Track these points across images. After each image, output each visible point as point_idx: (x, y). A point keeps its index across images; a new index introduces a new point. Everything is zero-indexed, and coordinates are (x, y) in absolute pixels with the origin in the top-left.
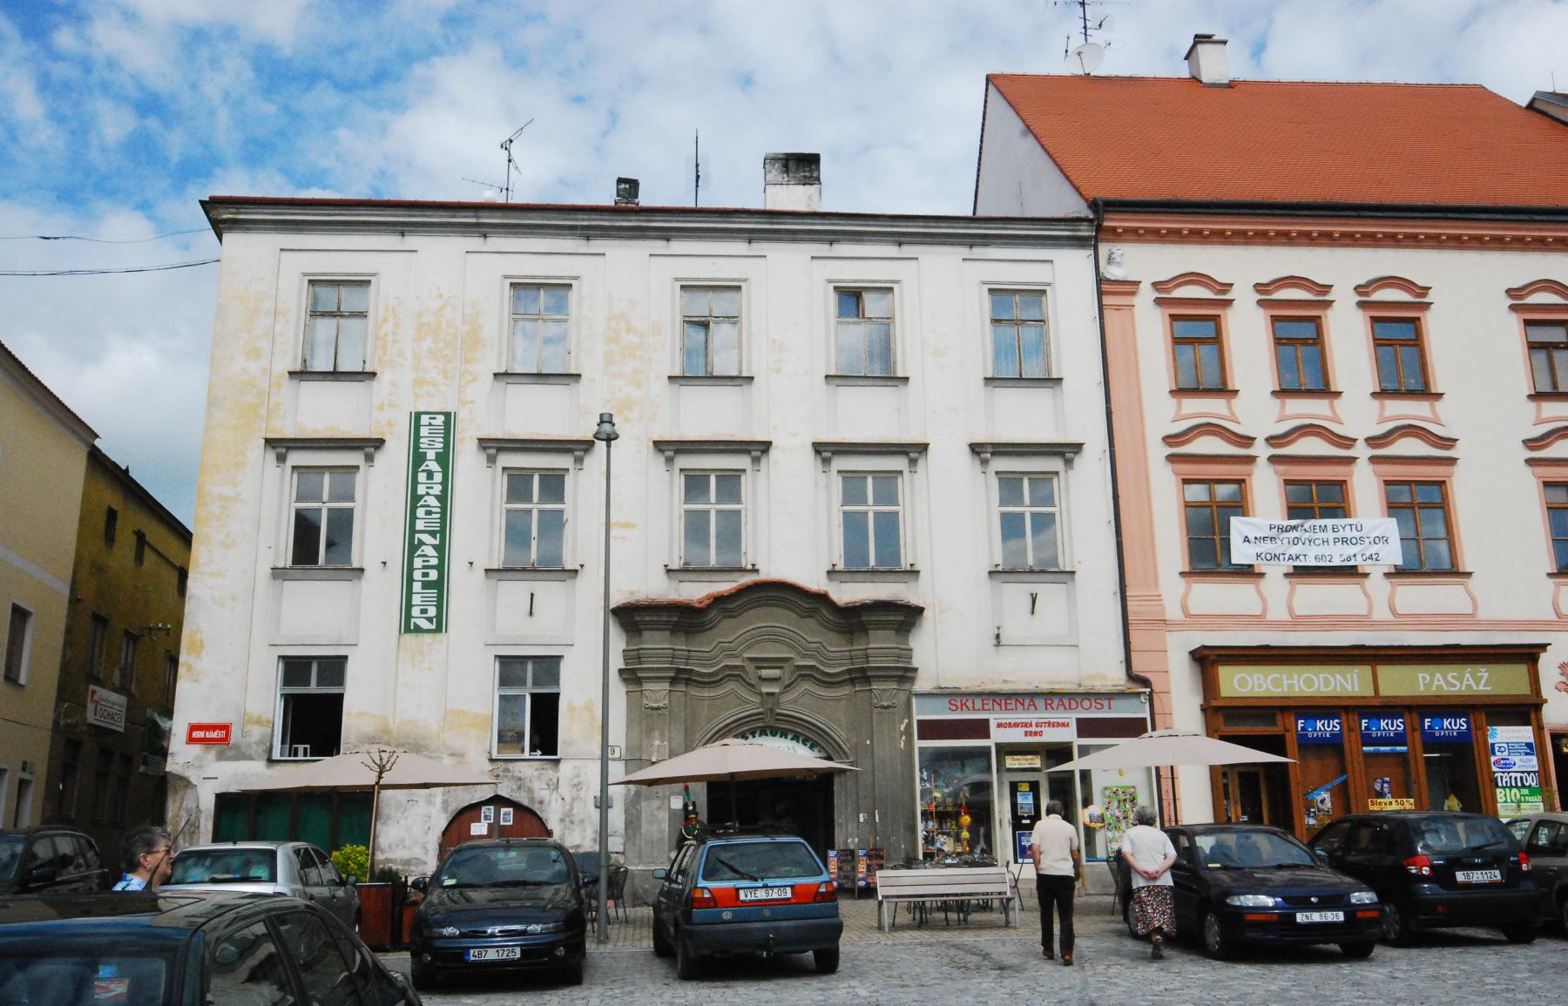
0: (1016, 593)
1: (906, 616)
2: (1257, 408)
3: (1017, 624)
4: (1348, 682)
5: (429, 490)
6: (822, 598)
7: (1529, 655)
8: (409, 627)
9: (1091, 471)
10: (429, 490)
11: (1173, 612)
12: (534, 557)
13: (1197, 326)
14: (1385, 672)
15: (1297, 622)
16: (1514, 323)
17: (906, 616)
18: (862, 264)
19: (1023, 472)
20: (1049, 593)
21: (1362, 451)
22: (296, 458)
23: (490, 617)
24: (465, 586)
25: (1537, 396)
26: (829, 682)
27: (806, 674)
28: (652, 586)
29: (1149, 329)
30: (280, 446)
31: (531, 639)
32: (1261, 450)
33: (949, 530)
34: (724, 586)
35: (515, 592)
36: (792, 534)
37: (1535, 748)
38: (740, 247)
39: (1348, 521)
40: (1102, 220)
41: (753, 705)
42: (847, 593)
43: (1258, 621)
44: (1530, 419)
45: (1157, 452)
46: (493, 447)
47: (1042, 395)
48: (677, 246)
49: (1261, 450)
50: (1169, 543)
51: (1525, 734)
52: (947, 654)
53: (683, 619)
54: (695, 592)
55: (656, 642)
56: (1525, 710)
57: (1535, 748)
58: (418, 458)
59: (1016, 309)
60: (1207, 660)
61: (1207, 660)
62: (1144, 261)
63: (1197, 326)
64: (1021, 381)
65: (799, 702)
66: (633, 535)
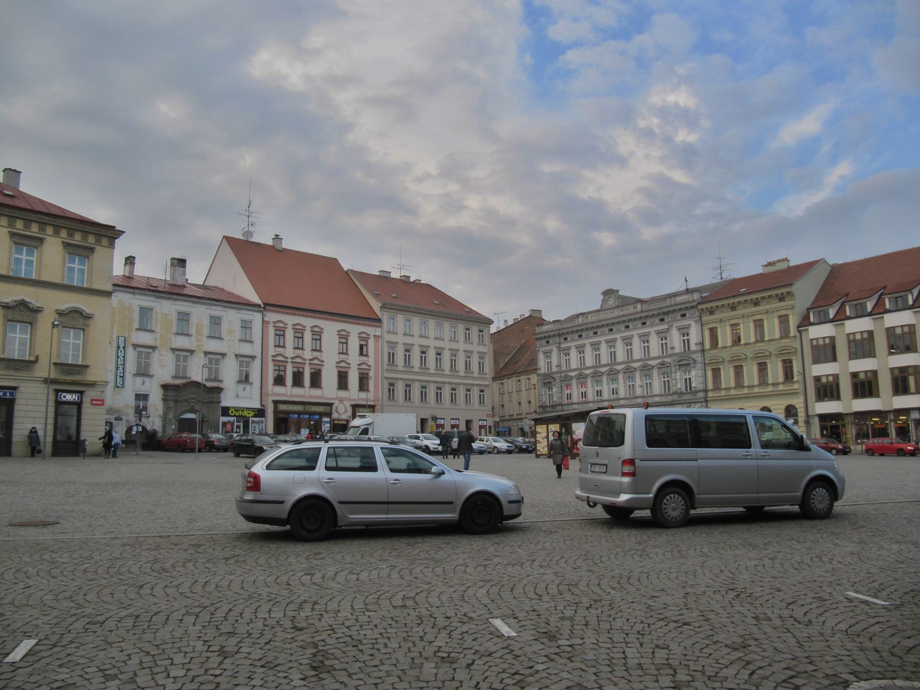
0: (241, 386)
1: (219, 390)
2: (289, 352)
3: (241, 393)
4: (299, 408)
5: (121, 354)
6: (204, 385)
7: (331, 405)
8: (117, 387)
9: (258, 362)
10: (121, 354)
11: (270, 392)
12: (143, 372)
13: (280, 333)
14: (307, 407)
15: (292, 396)
16: (337, 337)
17: (219, 390)
18: (217, 311)
19: (245, 359)
20: (147, 380)
21: (290, 360)
22: (209, 356)
23: (133, 385)
24: (129, 377)
25: (295, 348)
26: (203, 403)
27: (199, 401)
28: (169, 380)
29: (271, 332)
30: (174, 350)
31: (143, 390)
32: (307, 362)
33: (229, 373)
34: (184, 381)
35: (139, 380)
36: (197, 372)
37: (330, 422)
38: (222, 309)
39: (652, 411)
40: (267, 306)
41: (188, 407)
42: (209, 384)
43: (285, 395)
44: (337, 358)
45: (270, 359)
46: (135, 346)
47: (250, 344)
48: (178, 302)
49: (307, 362)
50: (271, 380)
51: (328, 419)
52: (227, 400)
53: (176, 388)
54: (178, 382)
55: (171, 393)
56: (329, 415)
57: (330, 422)
58: (119, 347)
59: (246, 326)
60: (276, 403)
61: (276, 403)
62: (272, 317)
63: (280, 333)
64: (182, 334)
65: (197, 407)
66: (164, 370)
